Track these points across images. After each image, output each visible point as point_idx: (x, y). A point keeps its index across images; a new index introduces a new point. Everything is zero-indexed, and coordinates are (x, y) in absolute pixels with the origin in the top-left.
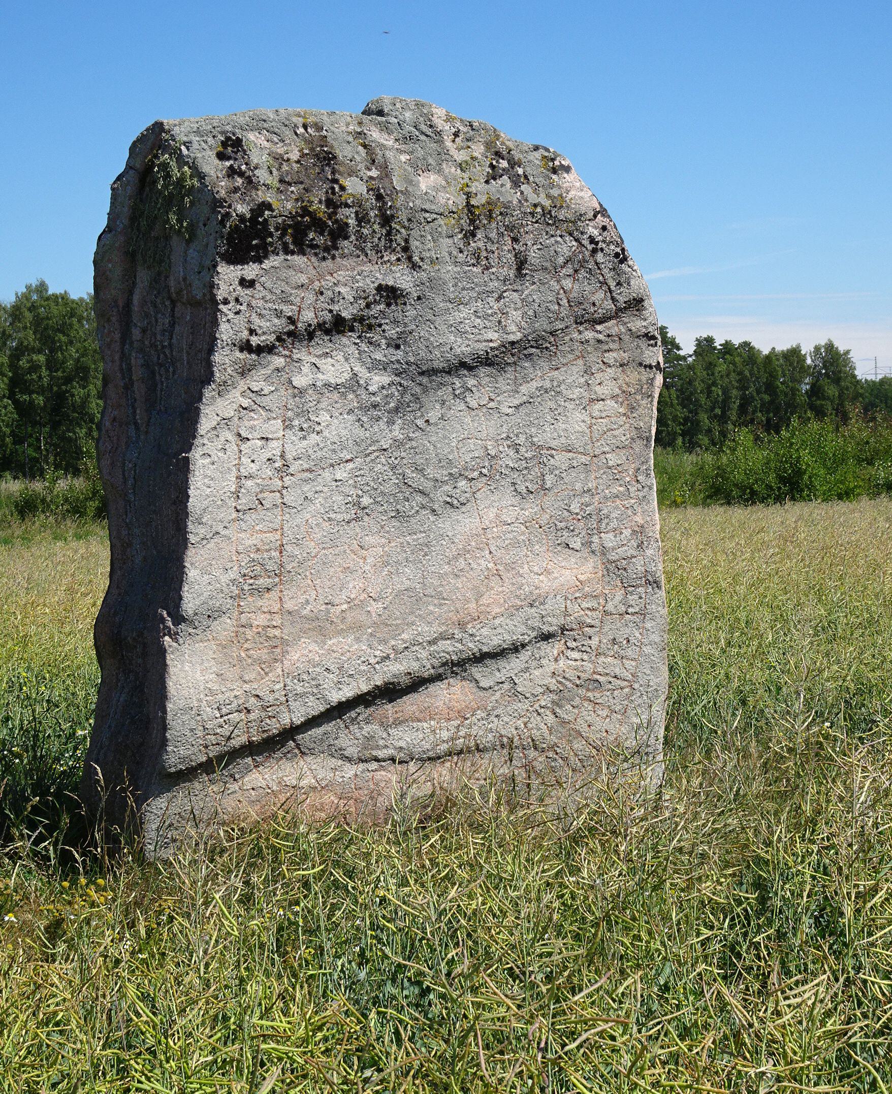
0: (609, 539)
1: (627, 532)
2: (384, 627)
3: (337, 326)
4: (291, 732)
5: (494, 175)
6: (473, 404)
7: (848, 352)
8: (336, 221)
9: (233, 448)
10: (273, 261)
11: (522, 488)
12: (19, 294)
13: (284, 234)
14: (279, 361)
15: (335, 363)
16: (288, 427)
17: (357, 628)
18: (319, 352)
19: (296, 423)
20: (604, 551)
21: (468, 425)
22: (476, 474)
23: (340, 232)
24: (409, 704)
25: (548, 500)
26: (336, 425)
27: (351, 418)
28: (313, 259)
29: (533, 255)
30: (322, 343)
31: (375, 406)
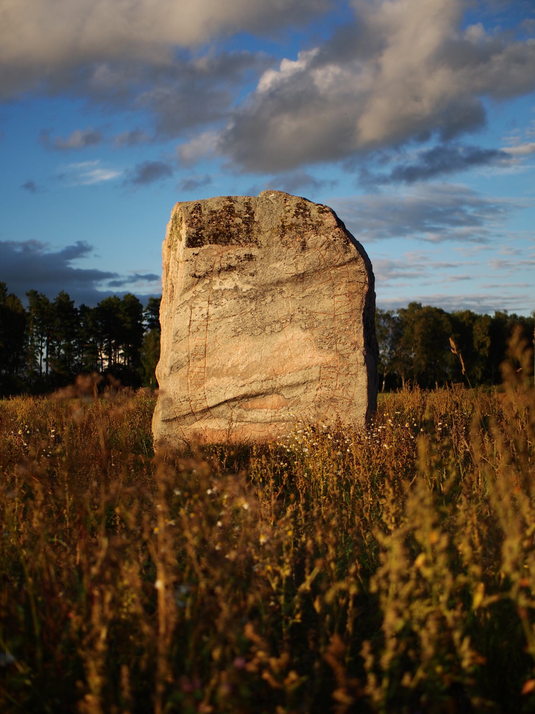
0: (340, 347)
1: (349, 344)
2: (245, 375)
3: (230, 268)
4: (209, 409)
5: (297, 214)
6: (285, 296)
7: (98, 304)
8: (230, 233)
9: (189, 311)
10: (206, 247)
11: (304, 326)
12: (79, 264)
13: (209, 237)
14: (207, 281)
15: (228, 282)
16: (210, 303)
17: (233, 375)
18: (223, 278)
19: (213, 302)
20: (337, 351)
21: (283, 305)
22: (284, 321)
23: (231, 236)
24: (257, 402)
25: (315, 332)
26: (228, 303)
27: (235, 301)
28: (220, 246)
29: (309, 243)
30: (223, 275)
31: (245, 297)
